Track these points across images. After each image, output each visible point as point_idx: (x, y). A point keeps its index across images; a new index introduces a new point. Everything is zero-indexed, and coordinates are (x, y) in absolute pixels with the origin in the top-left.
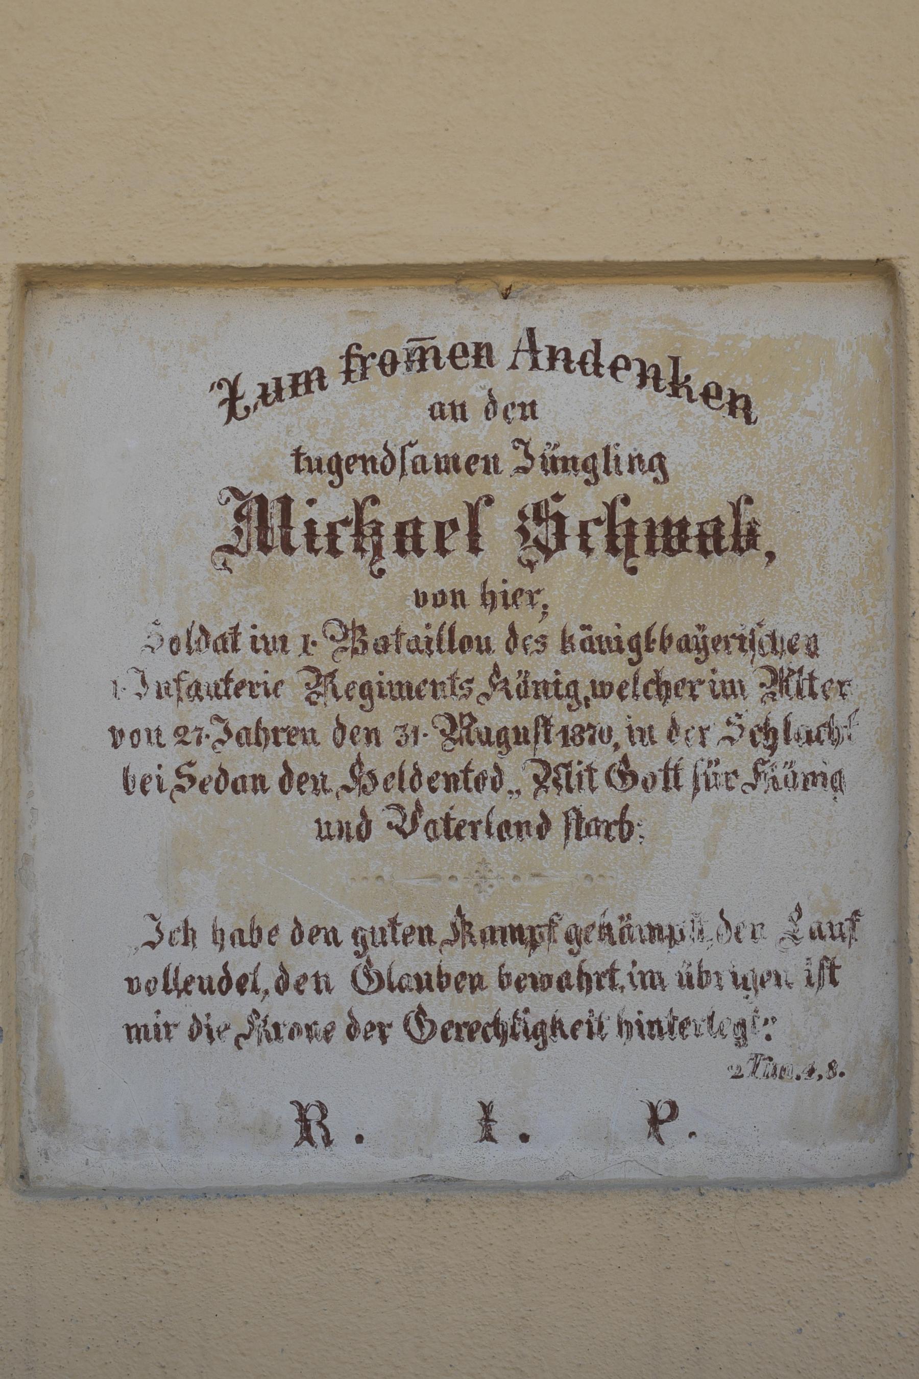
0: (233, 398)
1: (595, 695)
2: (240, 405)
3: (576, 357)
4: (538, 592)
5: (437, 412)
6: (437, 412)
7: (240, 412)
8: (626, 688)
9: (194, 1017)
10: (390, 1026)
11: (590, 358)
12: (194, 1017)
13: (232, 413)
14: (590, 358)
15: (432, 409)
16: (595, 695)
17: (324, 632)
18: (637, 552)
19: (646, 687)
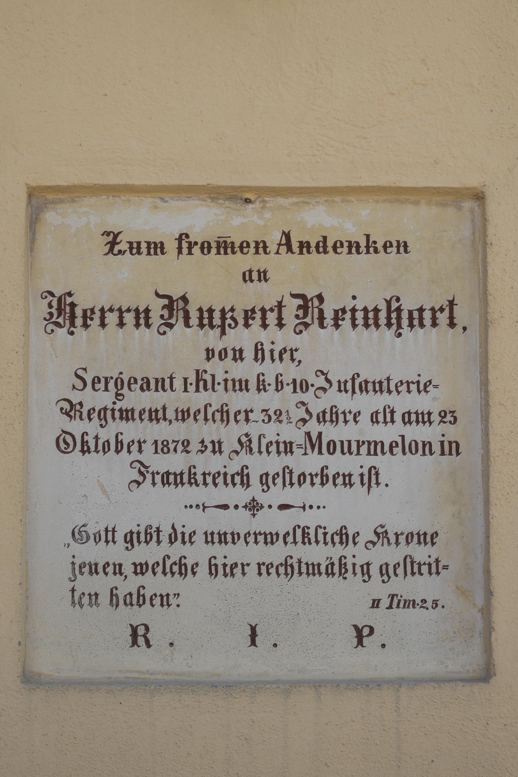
0: (113, 244)
1: (177, 419)
2: (117, 248)
3: (313, 245)
4: (296, 350)
5: (247, 277)
6: (247, 277)
7: (116, 251)
8: (144, 414)
9: (173, 527)
10: (248, 565)
11: (321, 244)
12: (173, 527)
13: (111, 250)
14: (321, 244)
15: (244, 274)
16: (177, 419)
17: (48, 334)
18: (393, 607)
19: (213, 414)
